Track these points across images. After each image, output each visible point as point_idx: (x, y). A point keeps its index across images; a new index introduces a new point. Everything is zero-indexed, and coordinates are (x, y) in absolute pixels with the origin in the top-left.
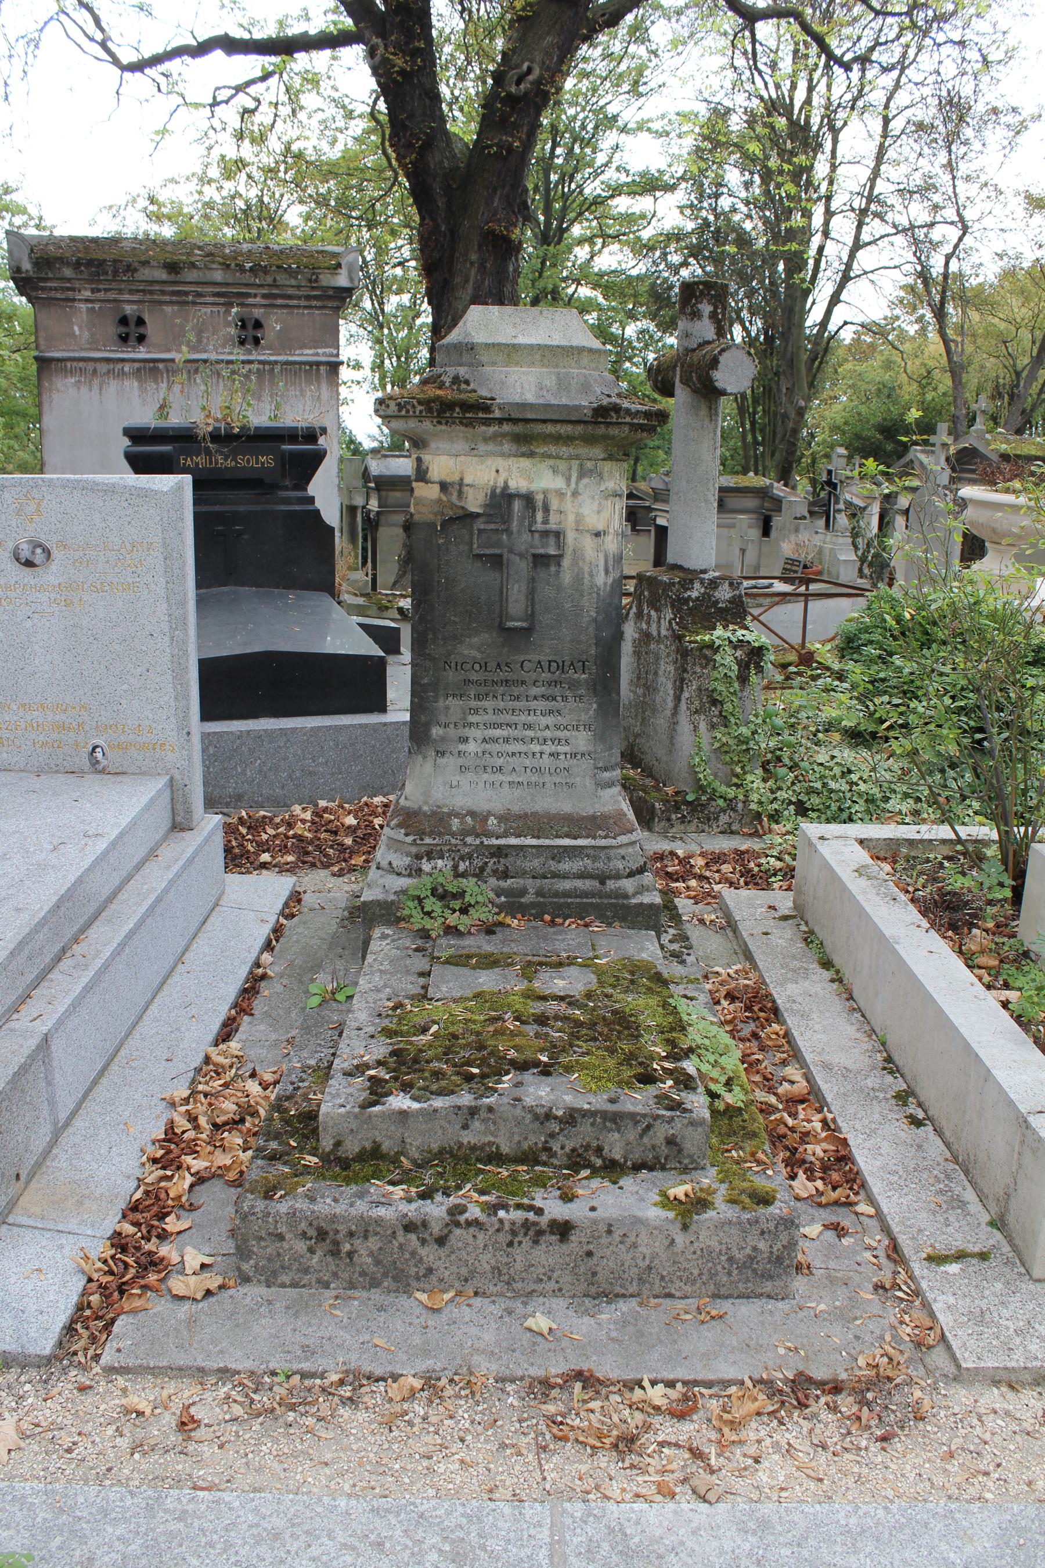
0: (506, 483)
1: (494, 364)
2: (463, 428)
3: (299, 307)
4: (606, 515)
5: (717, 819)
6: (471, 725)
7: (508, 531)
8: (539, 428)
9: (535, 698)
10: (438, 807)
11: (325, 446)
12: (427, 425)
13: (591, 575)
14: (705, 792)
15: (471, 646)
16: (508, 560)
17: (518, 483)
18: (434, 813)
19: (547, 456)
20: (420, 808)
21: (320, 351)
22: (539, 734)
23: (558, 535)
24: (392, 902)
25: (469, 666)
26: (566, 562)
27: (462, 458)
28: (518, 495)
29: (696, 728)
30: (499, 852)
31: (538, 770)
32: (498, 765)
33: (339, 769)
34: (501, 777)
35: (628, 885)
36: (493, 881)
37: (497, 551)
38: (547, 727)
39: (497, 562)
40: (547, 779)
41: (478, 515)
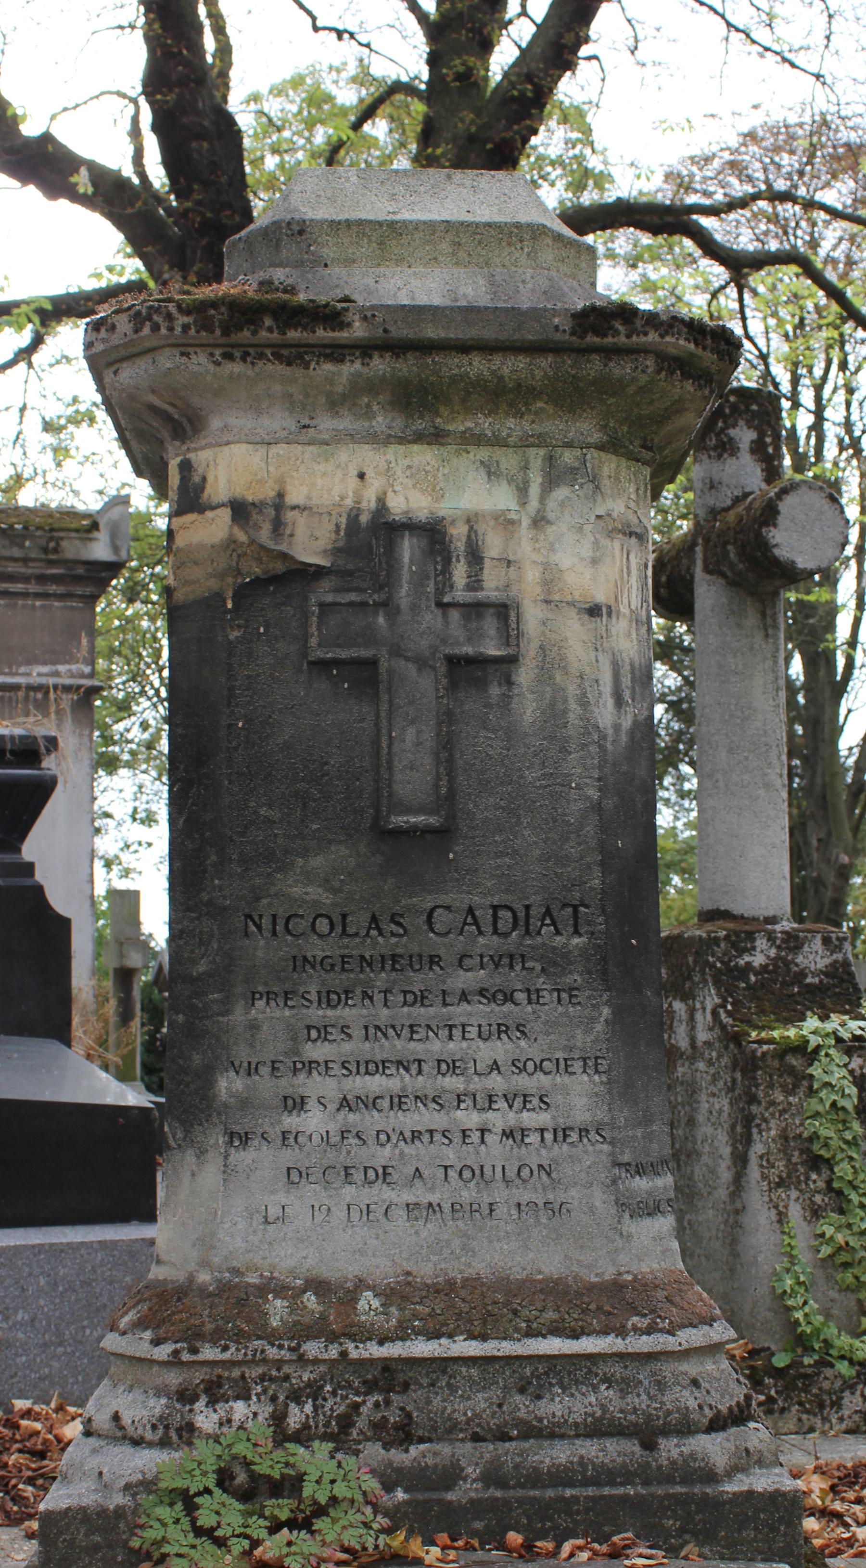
0: (381, 501)
1: (350, 262)
2: (280, 369)
3: (25, 595)
4: (611, 569)
5: (837, 1404)
6: (310, 1066)
7: (387, 605)
8: (454, 365)
9: (464, 997)
10: (236, 1271)
11: (55, 771)
12: (200, 361)
13: (584, 703)
14: (809, 1350)
15: (308, 877)
16: (390, 672)
17: (408, 501)
18: (224, 1288)
19: (476, 440)
20: (191, 1279)
21: (62, 668)
22: (477, 1084)
23: (504, 611)
24: (120, 1512)
25: (302, 925)
26: (524, 676)
27: (281, 449)
28: (410, 526)
29: (782, 1217)
30: (389, 1377)
31: (477, 1174)
34: (388, 1194)
35: (714, 1448)
36: (374, 1451)
37: (366, 653)
38: (495, 1066)
39: (364, 677)
40: (500, 1194)
41: (319, 572)
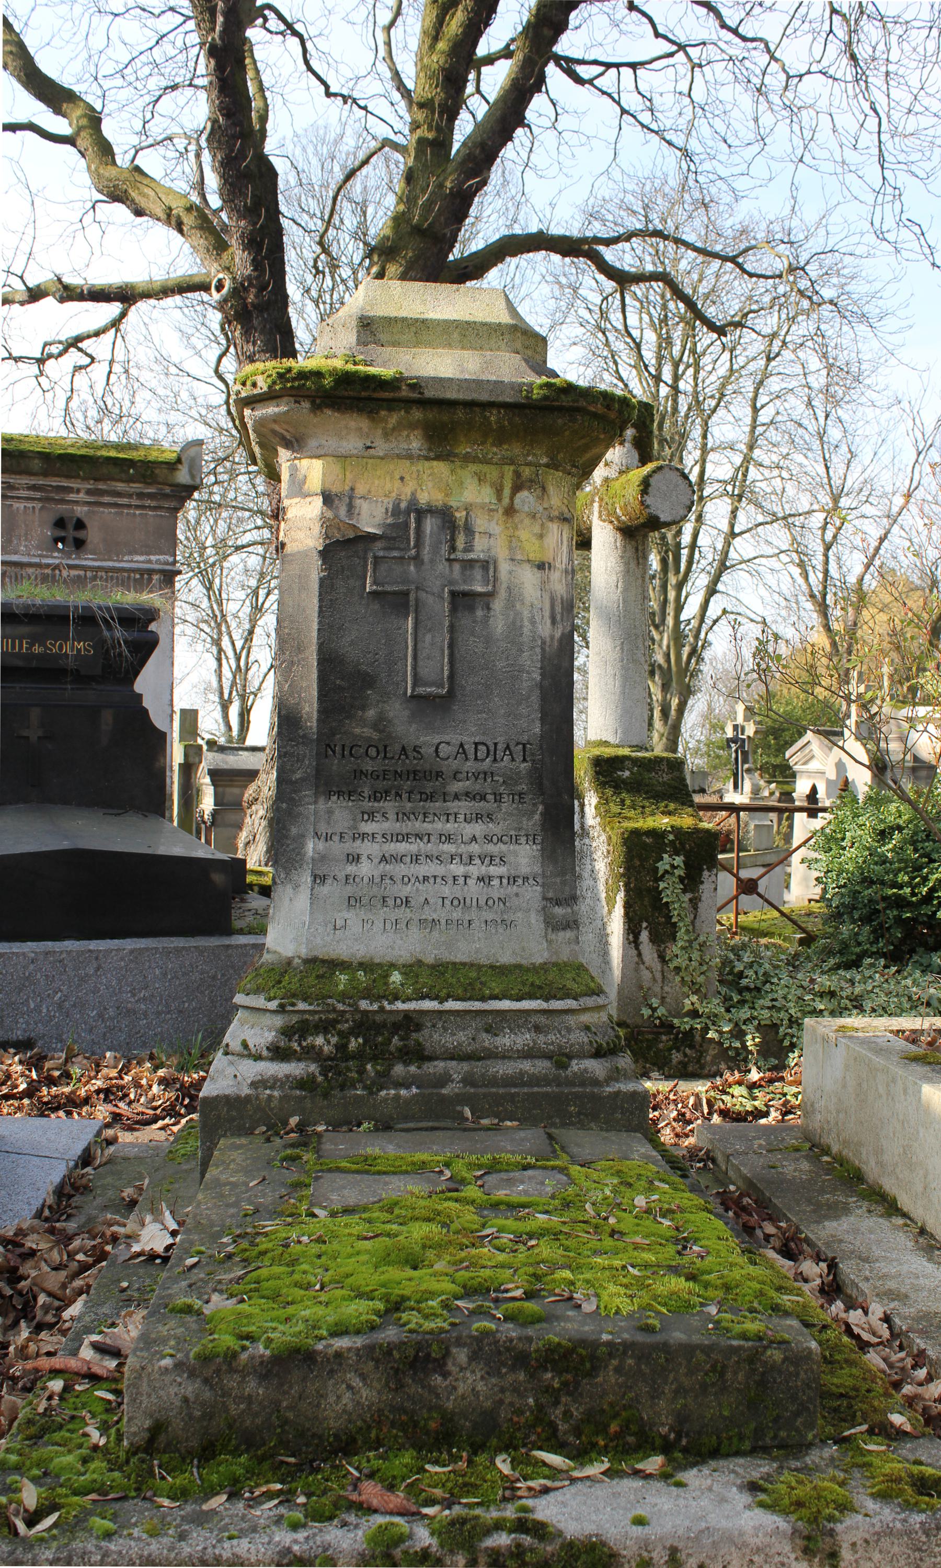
3: (129, 506)
6: (363, 836)
9: (456, 797)
13: (533, 622)
19: (467, 459)
21: (153, 558)
22: (463, 849)
26: (498, 605)
28: (431, 510)
30: (410, 1022)
32: (403, 895)
33: (167, 1005)
34: (408, 914)
38: (474, 839)
41: (371, 538)
